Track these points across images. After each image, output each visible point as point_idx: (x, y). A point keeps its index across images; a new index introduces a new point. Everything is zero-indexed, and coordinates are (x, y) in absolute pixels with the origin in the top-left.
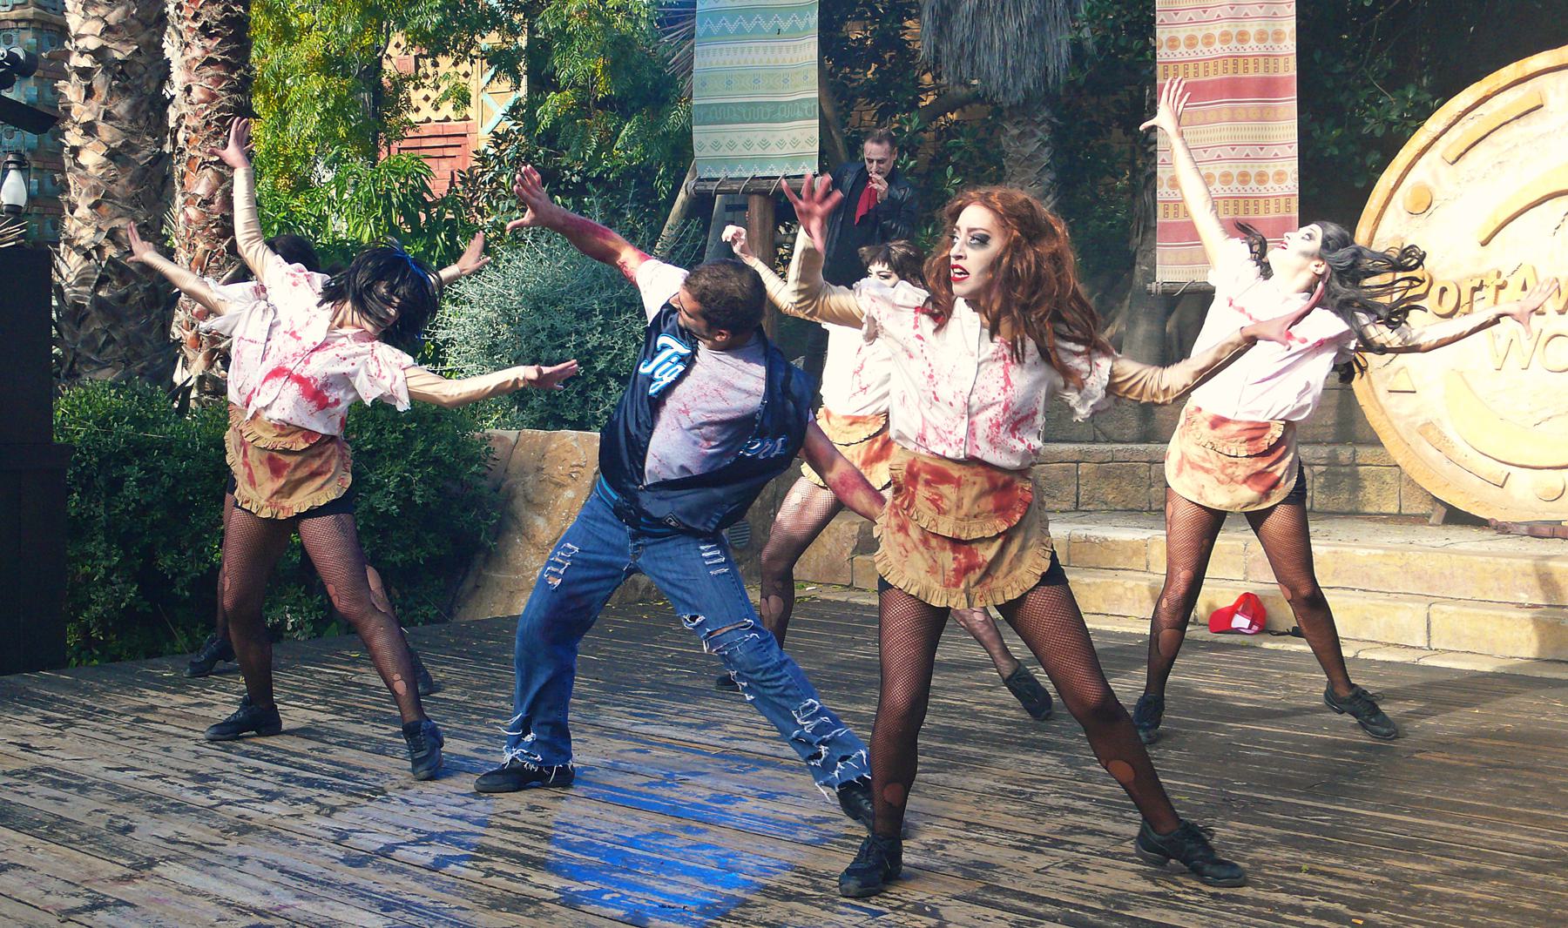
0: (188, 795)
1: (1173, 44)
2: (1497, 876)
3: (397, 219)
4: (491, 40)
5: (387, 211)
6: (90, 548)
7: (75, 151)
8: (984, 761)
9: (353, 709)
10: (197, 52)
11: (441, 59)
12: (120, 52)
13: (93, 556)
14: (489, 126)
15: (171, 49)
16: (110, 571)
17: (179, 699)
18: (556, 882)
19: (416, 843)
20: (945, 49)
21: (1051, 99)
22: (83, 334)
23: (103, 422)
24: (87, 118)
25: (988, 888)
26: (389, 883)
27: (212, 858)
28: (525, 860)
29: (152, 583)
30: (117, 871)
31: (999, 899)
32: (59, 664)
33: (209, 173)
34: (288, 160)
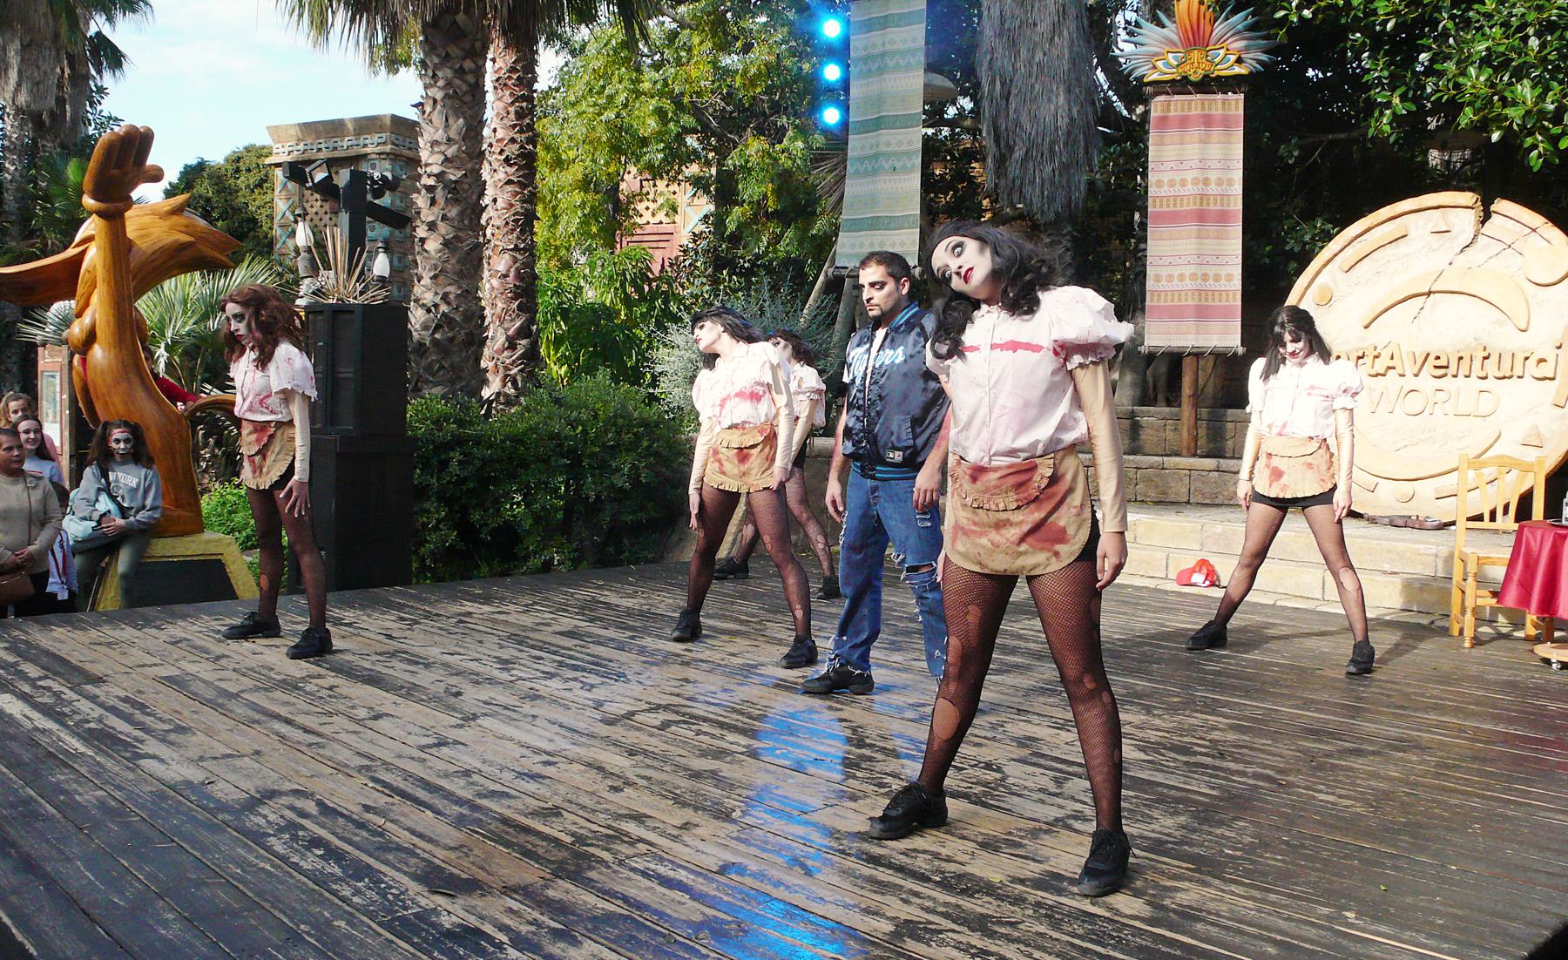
0: (496, 673)
1: (1159, 184)
2: (1373, 753)
3: (629, 289)
4: (693, 169)
5: (623, 285)
6: (426, 505)
7: (423, 240)
8: (1028, 668)
9: (602, 619)
10: (501, 176)
11: (658, 182)
12: (454, 175)
13: (428, 511)
14: (689, 227)
15: (485, 173)
16: (439, 521)
17: (486, 608)
18: (744, 740)
19: (649, 711)
20: (1003, 182)
21: (1072, 219)
22: (424, 363)
23: (437, 422)
24: (431, 219)
25: (1035, 754)
26: (632, 737)
27: (514, 715)
28: (722, 725)
29: (467, 531)
30: (454, 721)
31: (1042, 761)
32: (406, 582)
33: (507, 256)
34: (557, 248)
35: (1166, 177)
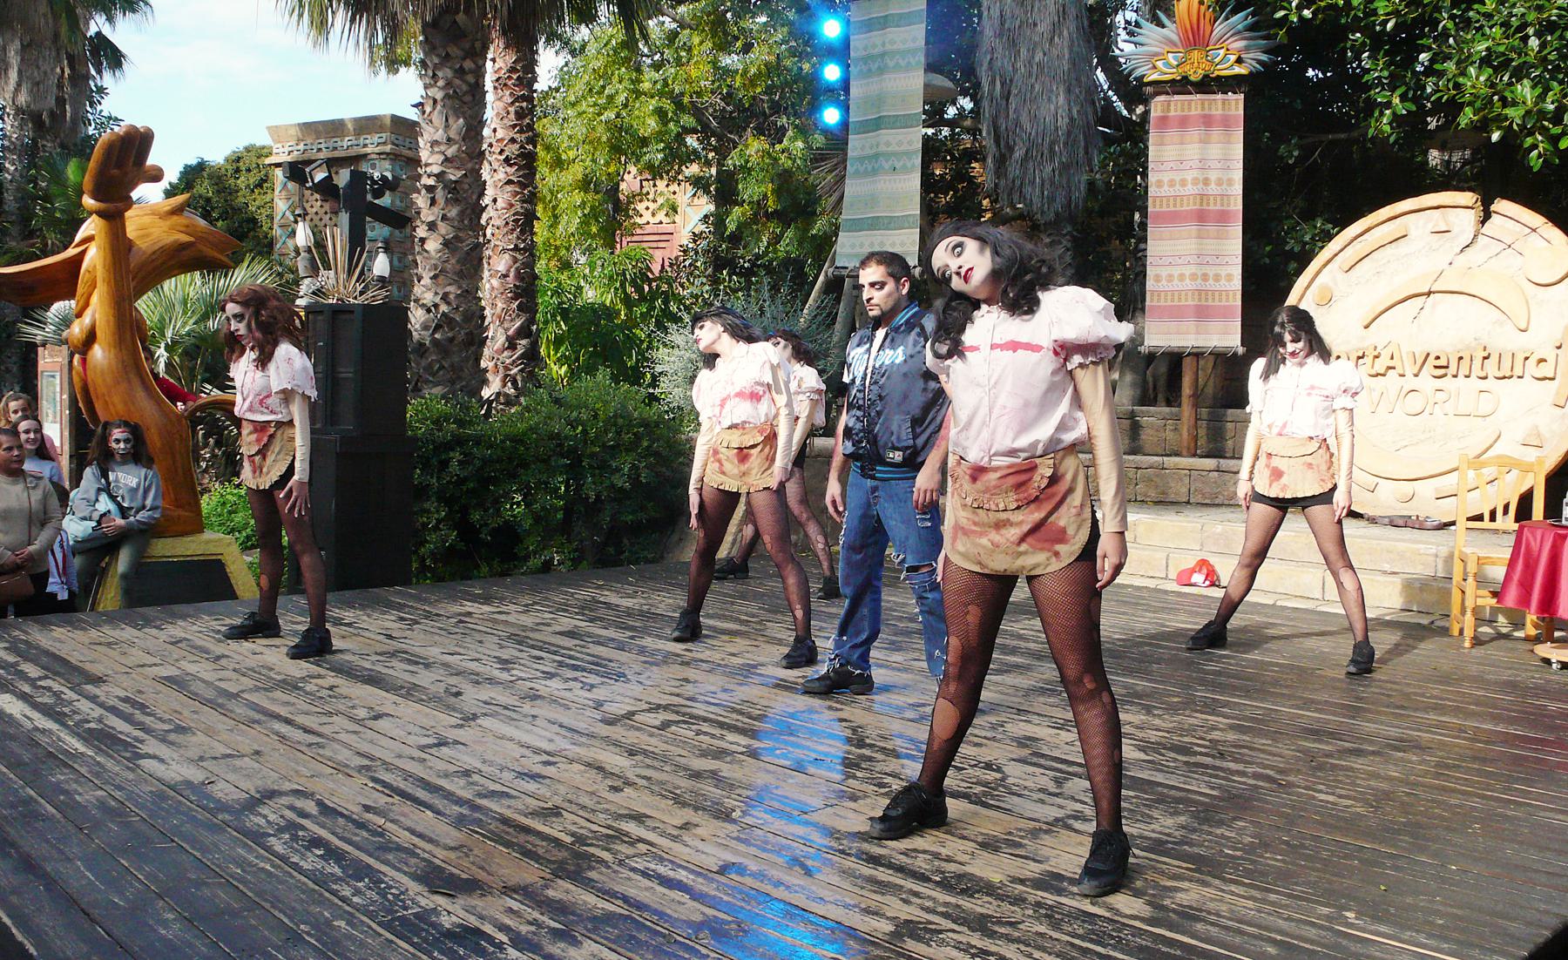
0: (496, 673)
1: (1159, 184)
2: (1373, 753)
3: (629, 289)
4: (693, 169)
5: (623, 285)
6: (426, 505)
7: (423, 240)
8: (1028, 668)
9: (602, 619)
10: (501, 176)
11: (658, 182)
12: (454, 175)
13: (428, 511)
14: (689, 227)
15: (485, 173)
16: (439, 521)
17: (486, 608)
18: (744, 740)
19: (649, 711)
20: (1003, 182)
21: (1072, 219)
22: (424, 363)
23: (437, 422)
24: (431, 219)
25: (1035, 754)
26: (632, 737)
27: (514, 715)
28: (722, 725)
29: (467, 531)
30: (454, 721)
31: (1042, 761)
32: (406, 582)
33: (507, 256)
34: (557, 248)
35: (1166, 177)
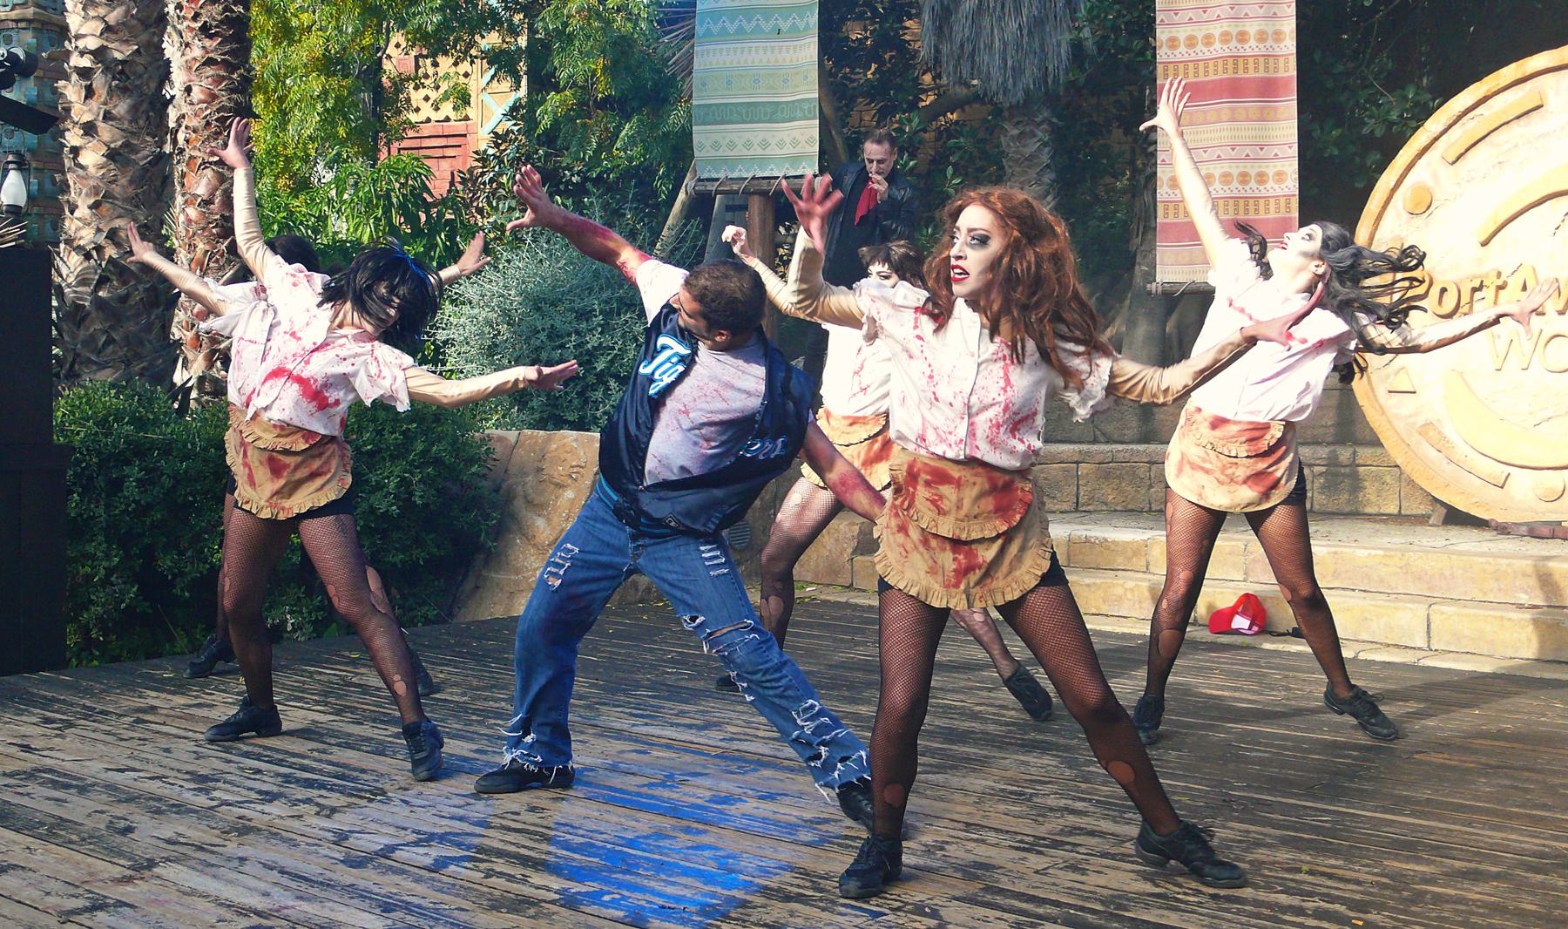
0: (188, 796)
1: (1173, 44)
2: (1497, 877)
3: (397, 220)
4: (491, 40)
5: (387, 211)
6: (90, 548)
7: (75, 151)
8: (984, 762)
9: (353, 710)
10: (197, 52)
11: (441, 59)
12: (120, 52)
13: (93, 557)
14: (489, 126)
15: (171, 49)
16: (110, 571)
17: (179, 700)
18: (556, 883)
19: (416, 844)
20: (945, 49)
21: (1051, 99)
22: (83, 334)
23: (103, 423)
24: (87, 118)
25: (988, 889)
26: (389, 884)
27: (212, 859)
28: (525, 861)
29: (152, 584)
30: (117, 872)
31: (999, 900)
32: (59, 664)
33: (209, 173)
34: (288, 160)
